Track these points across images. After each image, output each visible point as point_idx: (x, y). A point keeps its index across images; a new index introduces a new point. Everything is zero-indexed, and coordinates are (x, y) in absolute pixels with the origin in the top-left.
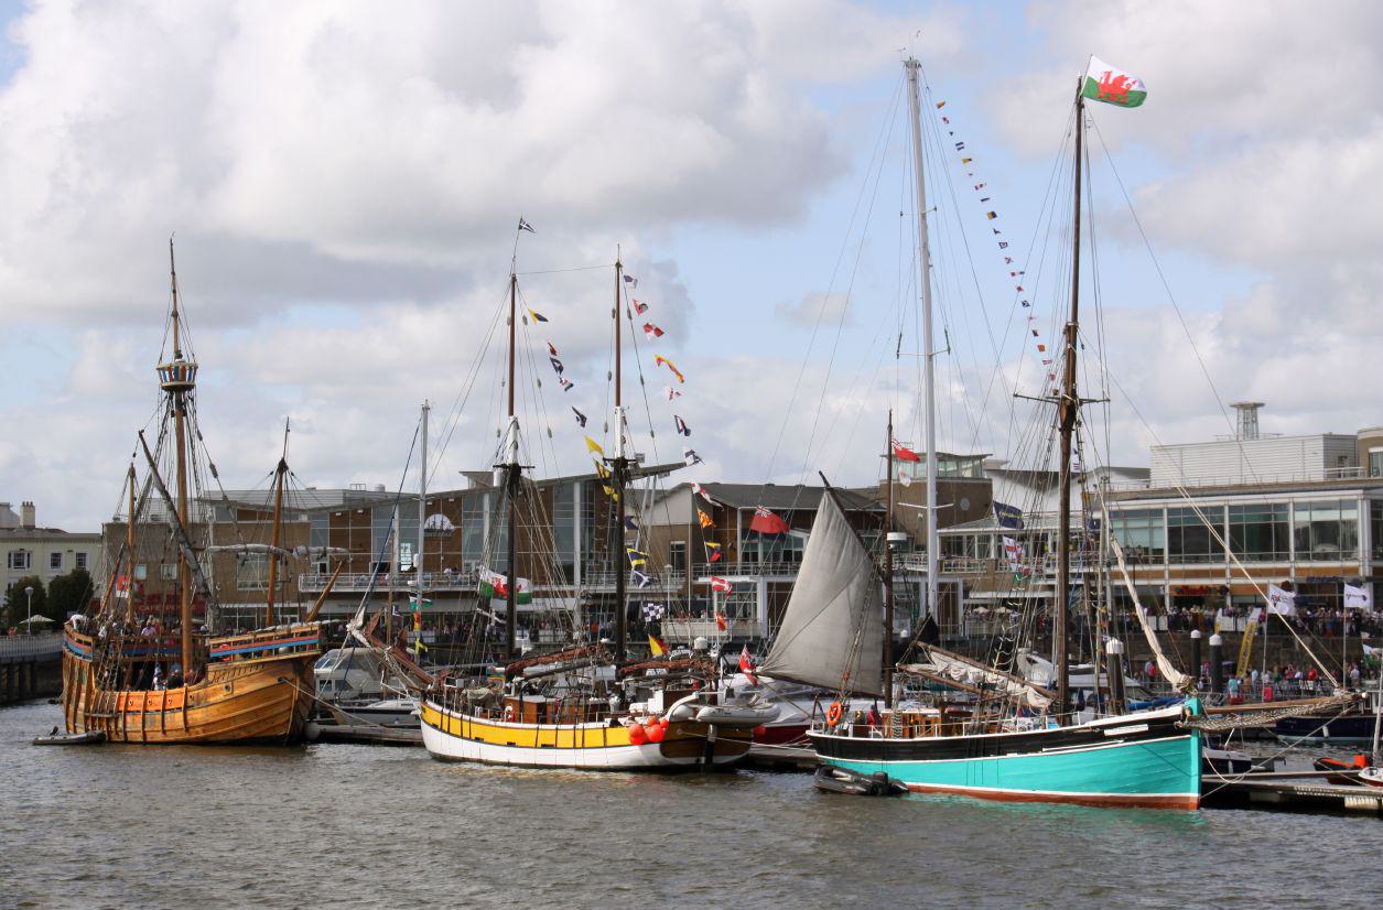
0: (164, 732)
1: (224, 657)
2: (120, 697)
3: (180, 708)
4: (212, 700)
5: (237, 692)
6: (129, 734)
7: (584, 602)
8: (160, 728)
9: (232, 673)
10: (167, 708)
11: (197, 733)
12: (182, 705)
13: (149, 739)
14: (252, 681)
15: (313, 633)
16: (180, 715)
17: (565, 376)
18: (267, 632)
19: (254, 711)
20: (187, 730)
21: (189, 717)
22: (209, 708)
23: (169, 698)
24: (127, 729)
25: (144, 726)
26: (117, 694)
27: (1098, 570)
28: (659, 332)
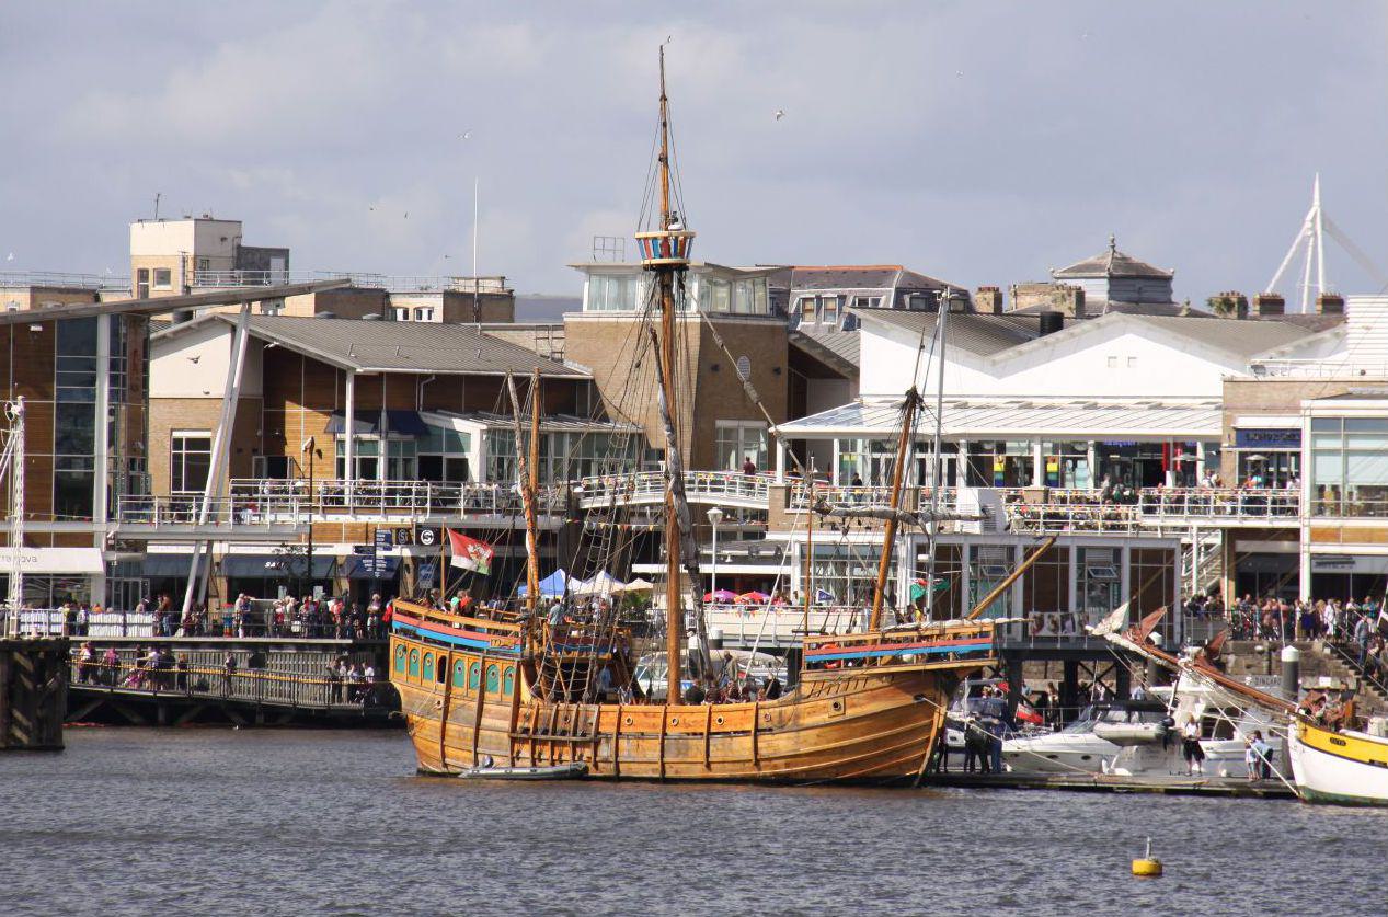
0: (708, 765)
1: (831, 662)
2: (578, 712)
3: (702, 734)
4: (808, 721)
5: (851, 713)
6: (622, 766)
7: (114, 557)
8: (701, 758)
9: (843, 685)
10: (713, 730)
11: (775, 767)
12: (750, 727)
13: (670, 774)
14: (874, 698)
15: (983, 634)
16: (748, 741)
17: (1303, 303)
18: (905, 630)
19: (875, 740)
20: (757, 763)
21: (760, 745)
22: (802, 733)
23: (762, 712)
24: (620, 759)
25: (662, 756)
26: (574, 707)
27: (514, 424)
28: (778, 117)
